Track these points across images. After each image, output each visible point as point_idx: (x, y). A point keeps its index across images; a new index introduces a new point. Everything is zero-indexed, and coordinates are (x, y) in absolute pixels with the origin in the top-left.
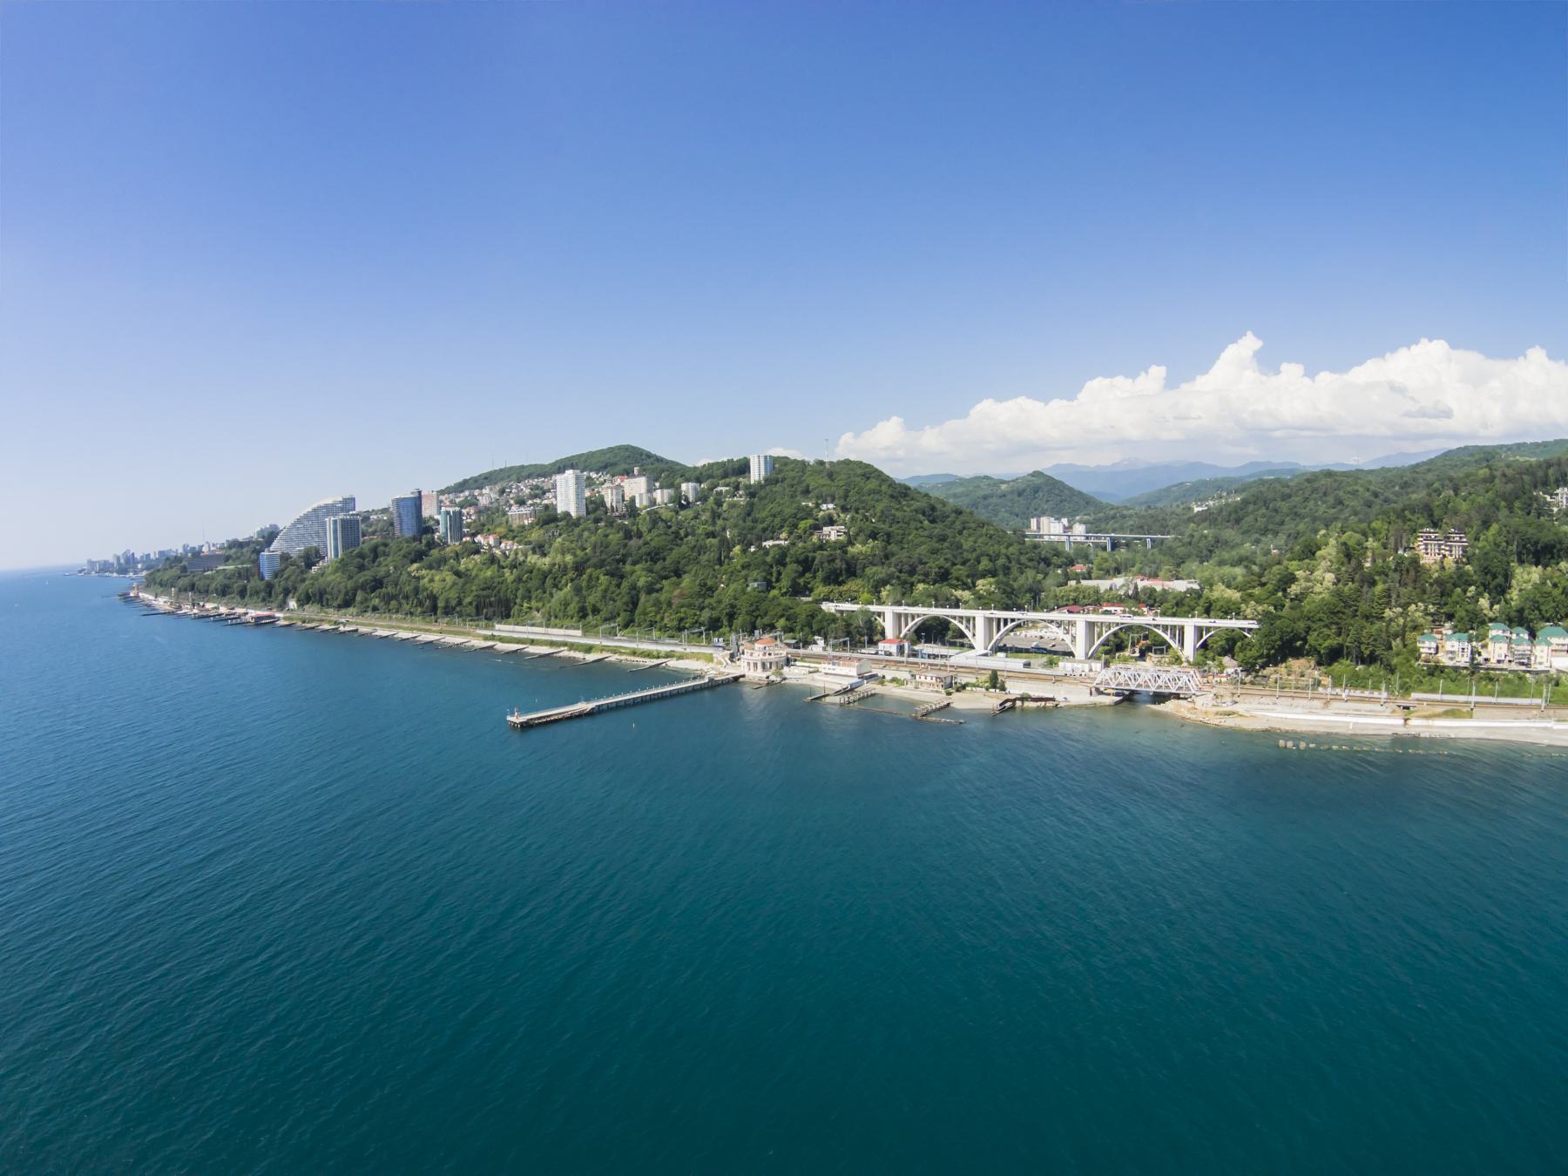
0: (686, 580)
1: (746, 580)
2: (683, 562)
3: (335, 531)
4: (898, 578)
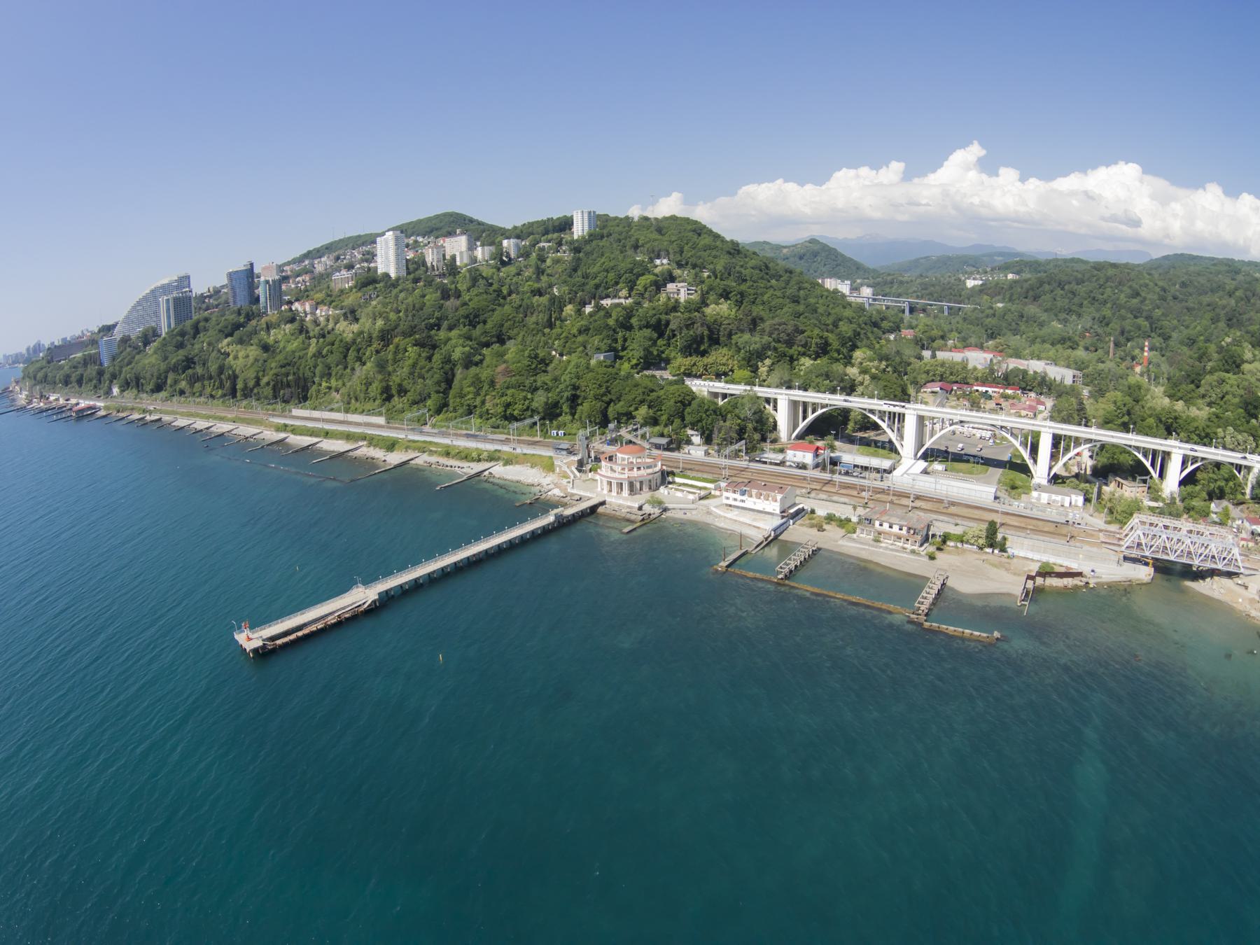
0: (512, 347)
1: (585, 347)
2: (507, 325)
3: (168, 310)
4: (775, 349)
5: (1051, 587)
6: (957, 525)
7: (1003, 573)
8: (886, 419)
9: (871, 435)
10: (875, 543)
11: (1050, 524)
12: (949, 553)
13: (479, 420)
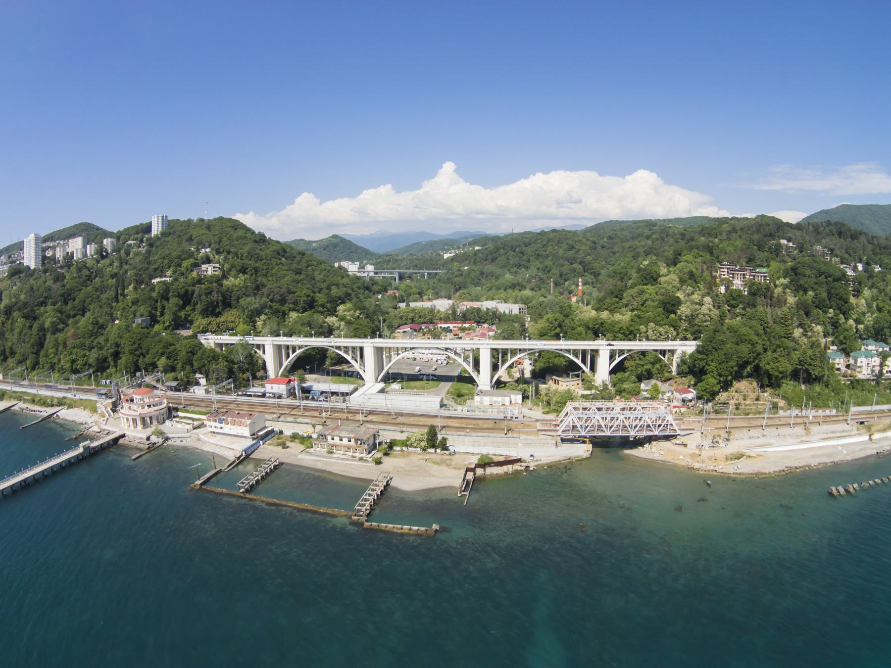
1: (135, 315)
4: (271, 307)
5: (492, 475)
6: (402, 432)
7: (444, 468)
8: (350, 352)
9: (345, 367)
10: (329, 455)
11: (489, 421)
12: (395, 456)
13: (58, 375)
